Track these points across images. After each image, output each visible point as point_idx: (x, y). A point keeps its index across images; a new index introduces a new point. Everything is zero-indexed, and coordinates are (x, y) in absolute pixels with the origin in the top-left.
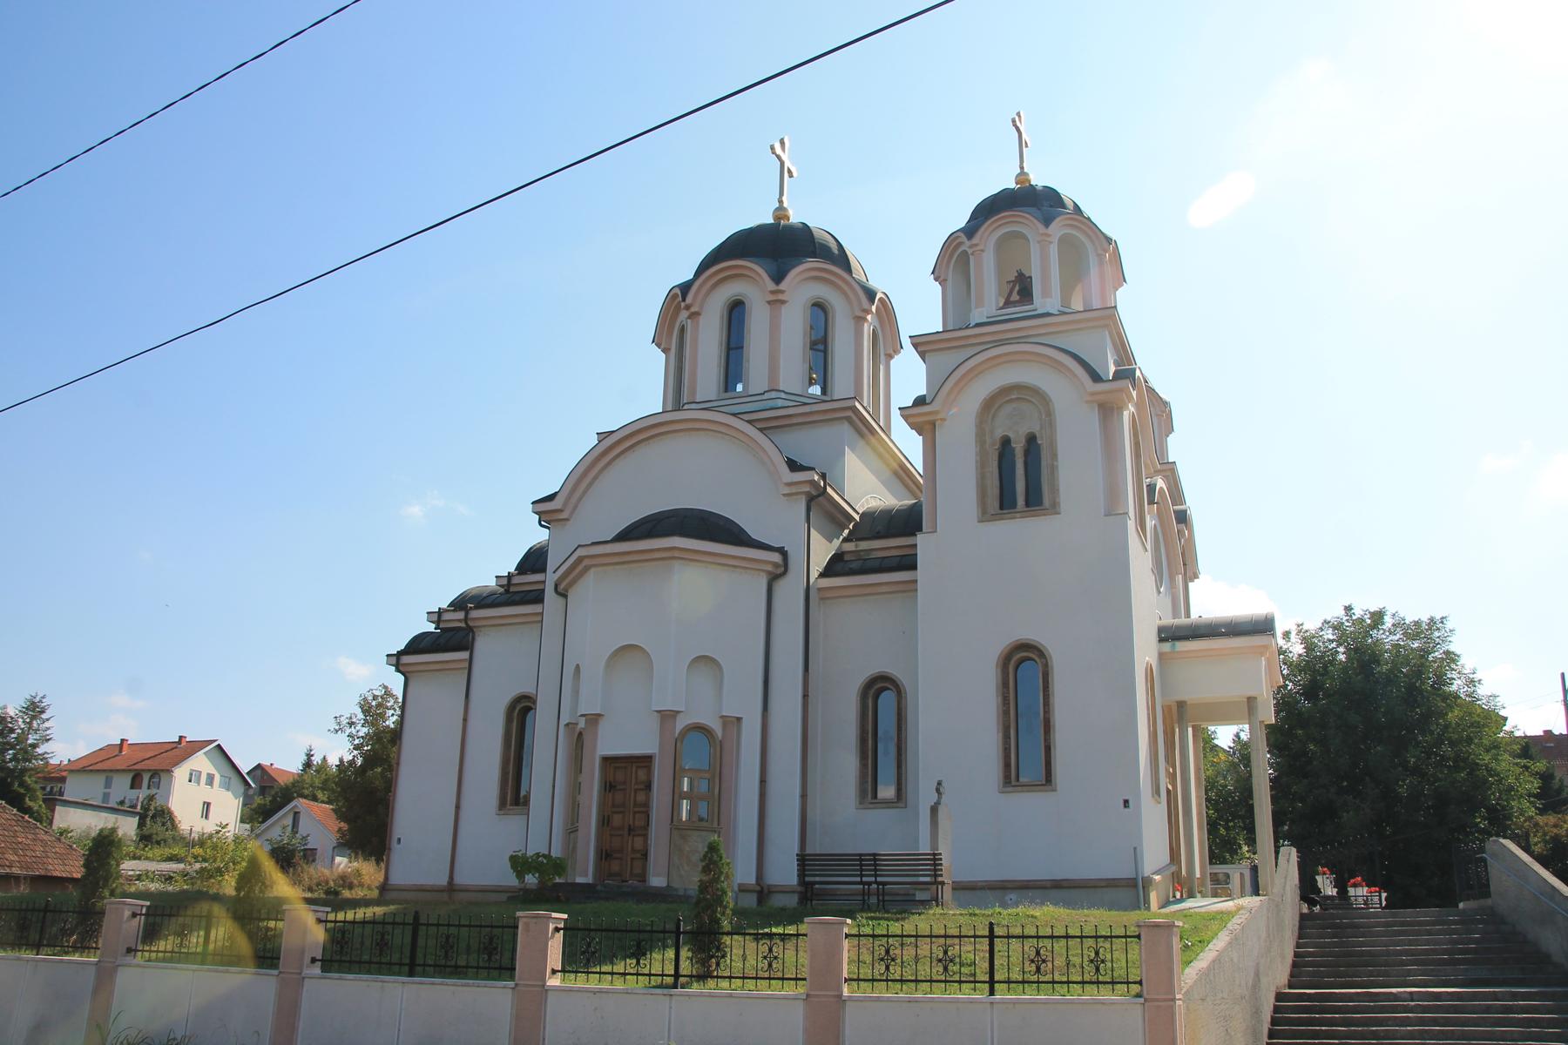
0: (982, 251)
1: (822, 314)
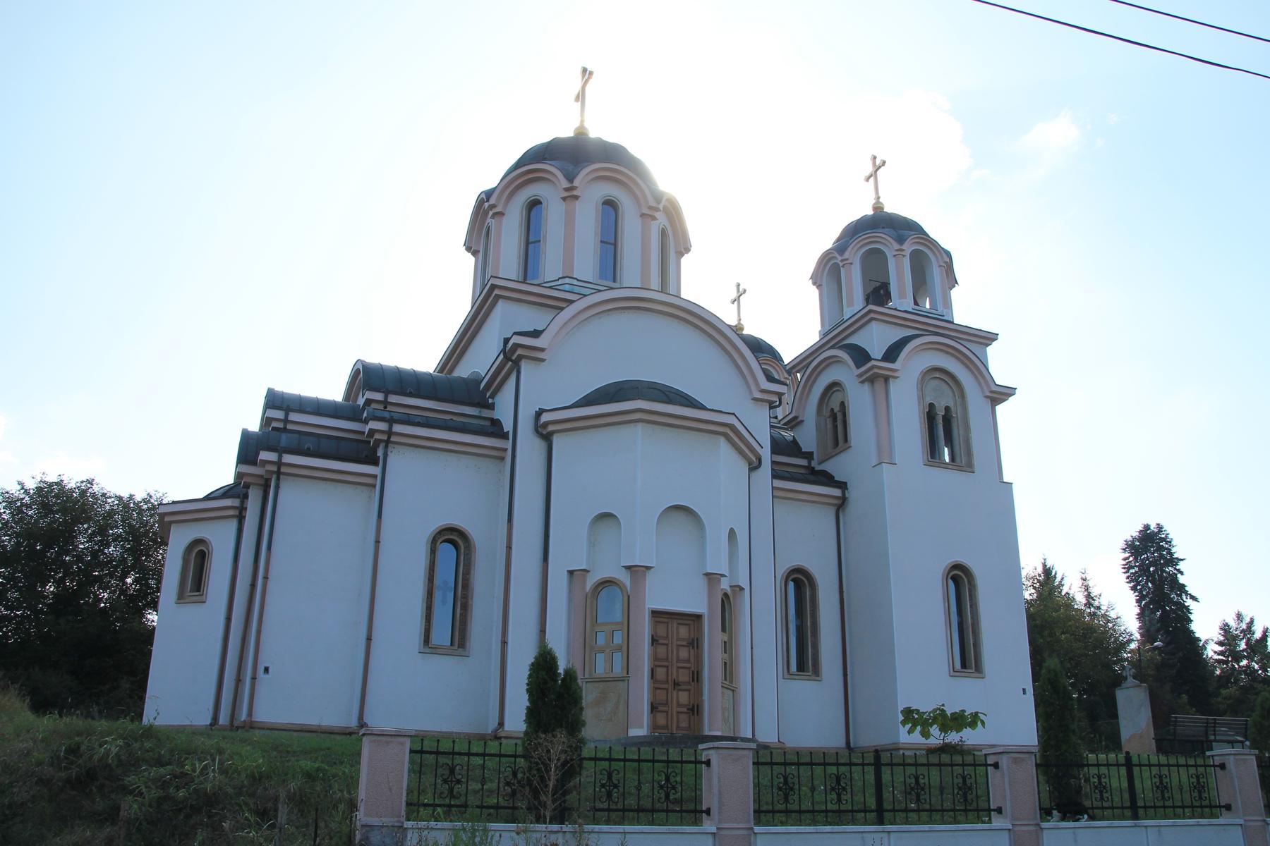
0: (851, 264)
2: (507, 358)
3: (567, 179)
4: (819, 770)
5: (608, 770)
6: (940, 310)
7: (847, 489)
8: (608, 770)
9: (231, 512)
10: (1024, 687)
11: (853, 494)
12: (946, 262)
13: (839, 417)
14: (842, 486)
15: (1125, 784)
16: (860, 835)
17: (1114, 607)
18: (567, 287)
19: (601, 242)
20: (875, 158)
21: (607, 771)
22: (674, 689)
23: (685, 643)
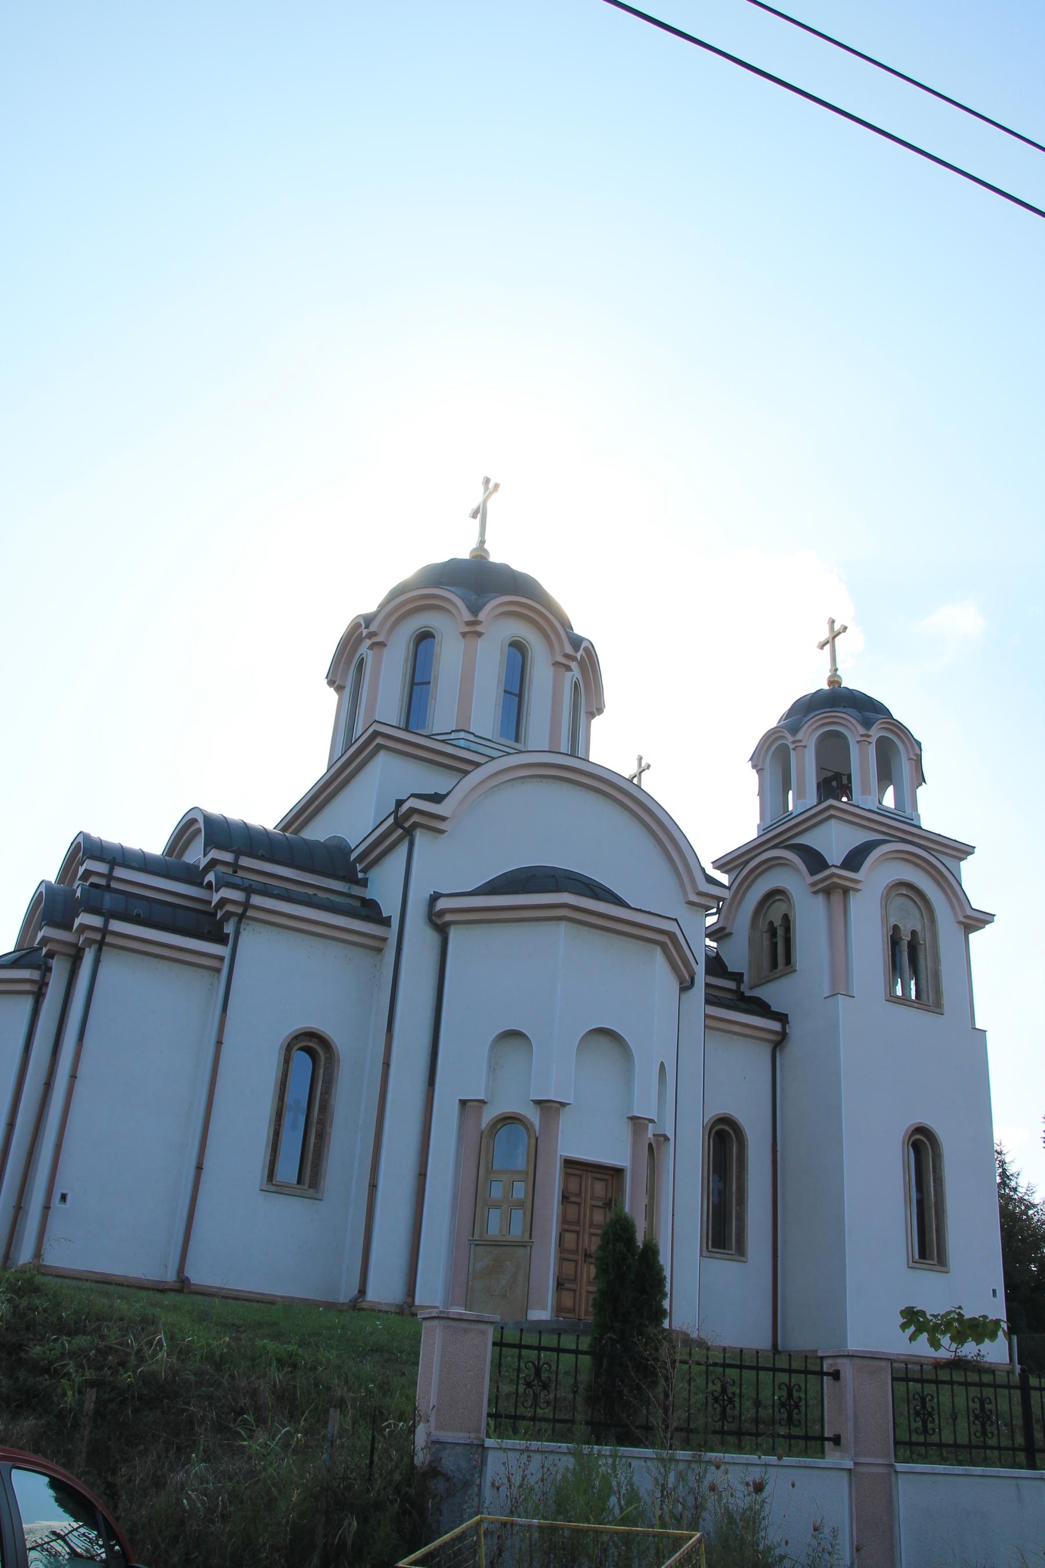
0: (805, 747)
1: (519, 656)
2: (398, 824)
3: (469, 610)
4: (765, 1377)
5: (788, 1384)
6: (908, 812)
7: (788, 1023)
8: (788, 1384)
9: (27, 987)
10: (994, 1288)
11: (795, 1029)
12: (916, 755)
13: (780, 932)
14: (782, 1018)
15: (1018, 1410)
16: (1014, 1482)
17: (1034, 1190)
18: (462, 743)
19: (505, 691)
20: (833, 622)
21: (978, 1398)
22: (585, 1262)
23: (600, 1204)
